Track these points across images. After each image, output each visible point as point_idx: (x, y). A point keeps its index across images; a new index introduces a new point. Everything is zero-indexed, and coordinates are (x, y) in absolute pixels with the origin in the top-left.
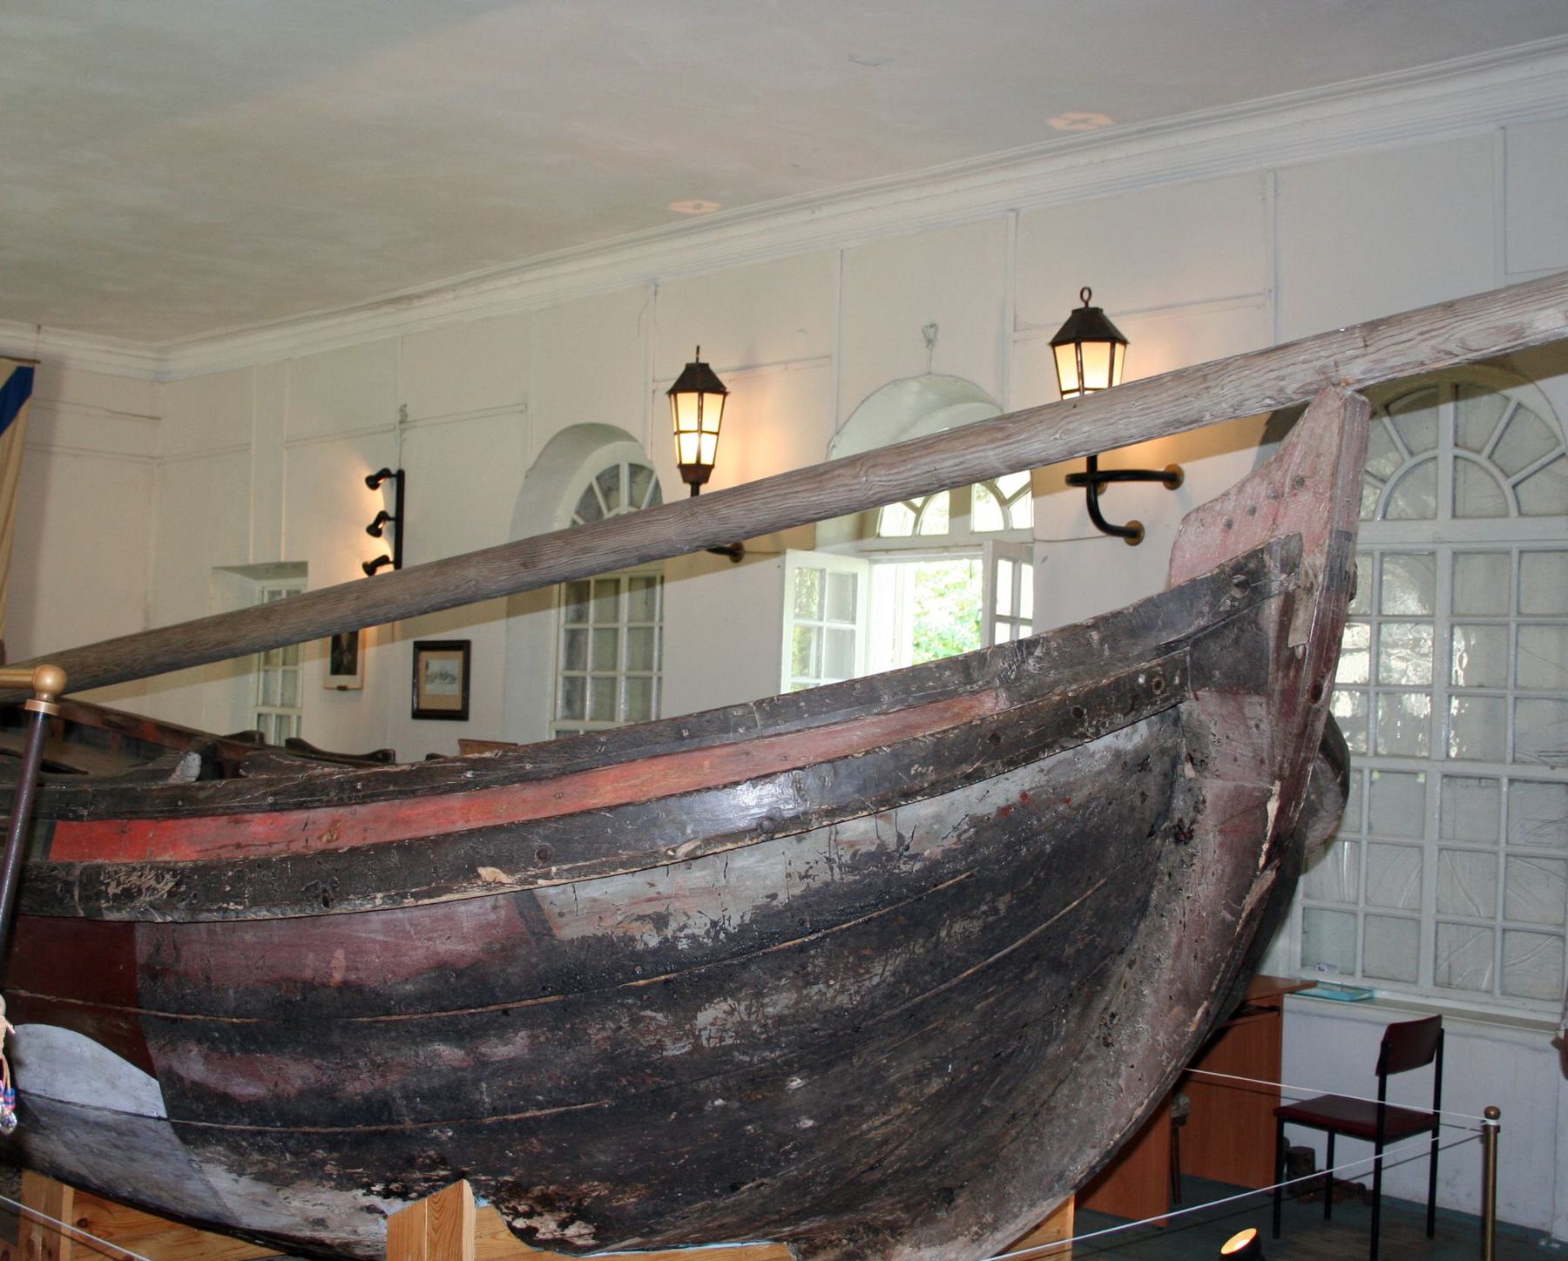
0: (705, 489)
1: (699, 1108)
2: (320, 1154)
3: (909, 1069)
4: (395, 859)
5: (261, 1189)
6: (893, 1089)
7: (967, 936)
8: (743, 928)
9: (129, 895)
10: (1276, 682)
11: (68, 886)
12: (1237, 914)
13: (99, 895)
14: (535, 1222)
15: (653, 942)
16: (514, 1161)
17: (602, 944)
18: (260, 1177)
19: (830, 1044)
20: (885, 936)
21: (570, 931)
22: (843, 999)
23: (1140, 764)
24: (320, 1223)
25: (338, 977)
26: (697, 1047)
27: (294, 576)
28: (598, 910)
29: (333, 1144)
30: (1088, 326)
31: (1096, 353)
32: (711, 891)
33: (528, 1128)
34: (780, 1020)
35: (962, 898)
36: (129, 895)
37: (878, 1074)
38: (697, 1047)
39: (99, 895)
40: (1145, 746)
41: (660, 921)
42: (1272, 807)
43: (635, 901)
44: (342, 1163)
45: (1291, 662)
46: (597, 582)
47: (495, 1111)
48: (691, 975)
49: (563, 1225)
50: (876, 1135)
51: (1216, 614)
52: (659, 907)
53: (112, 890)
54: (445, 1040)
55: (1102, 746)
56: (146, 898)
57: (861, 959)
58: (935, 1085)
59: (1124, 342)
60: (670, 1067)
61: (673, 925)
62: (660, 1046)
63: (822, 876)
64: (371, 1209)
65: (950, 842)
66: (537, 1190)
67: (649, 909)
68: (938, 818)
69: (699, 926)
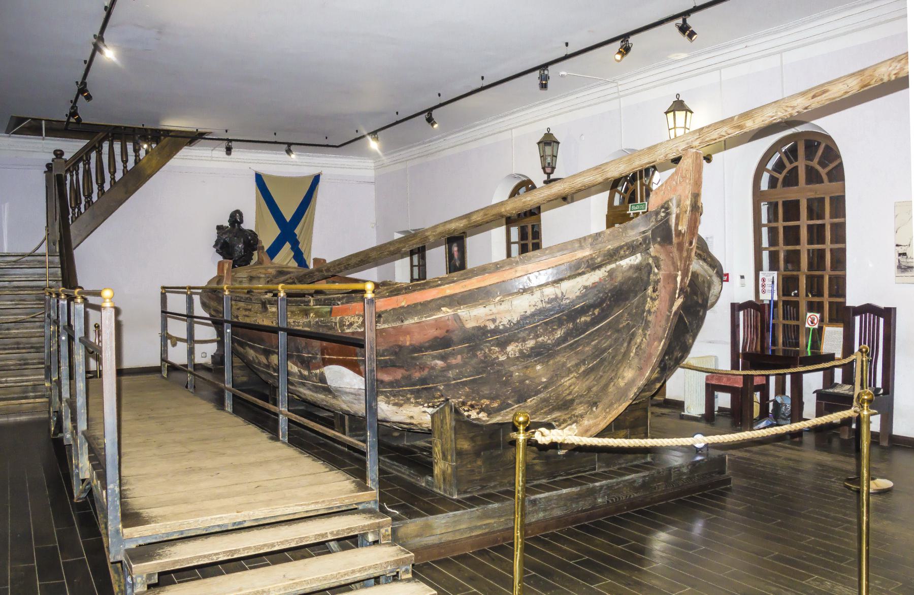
0: (552, 177)
1: (511, 376)
2: (409, 396)
3: (573, 363)
4: (419, 307)
5: (395, 408)
6: (569, 369)
7: (586, 322)
8: (518, 322)
9: (351, 324)
10: (675, 240)
11: (336, 323)
12: (671, 312)
13: (344, 325)
14: (470, 413)
15: (493, 327)
16: (462, 395)
17: (479, 328)
18: (395, 404)
19: (541, 353)
20: (560, 322)
21: (470, 325)
22: (549, 342)
23: (638, 268)
24: (412, 417)
25: (408, 344)
26: (508, 357)
27: (293, 291)
28: (477, 318)
29: (412, 392)
30: (679, 105)
31: (680, 115)
32: (508, 311)
33: (464, 384)
34: (532, 348)
35: (583, 311)
36: (351, 324)
37: (564, 364)
38: (508, 357)
39: (344, 325)
40: (641, 263)
41: (494, 320)
42: (679, 279)
43: (486, 315)
44: (416, 398)
45: (679, 233)
46: (778, 179)
47: (454, 379)
48: (504, 337)
49: (478, 413)
50: (567, 384)
51: (657, 221)
52: (493, 317)
53: (347, 323)
54: (438, 359)
55: (625, 263)
56: (356, 324)
57: (554, 330)
58: (583, 369)
59: (691, 112)
60: (501, 364)
61: (498, 322)
62: (498, 358)
63: (540, 306)
64: (424, 412)
65: (578, 294)
66: (469, 403)
67: (491, 317)
68: (573, 287)
69: (505, 322)
